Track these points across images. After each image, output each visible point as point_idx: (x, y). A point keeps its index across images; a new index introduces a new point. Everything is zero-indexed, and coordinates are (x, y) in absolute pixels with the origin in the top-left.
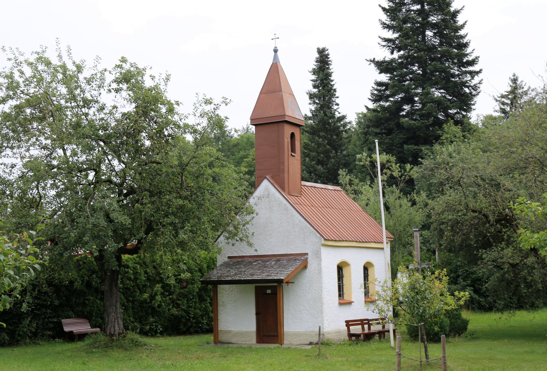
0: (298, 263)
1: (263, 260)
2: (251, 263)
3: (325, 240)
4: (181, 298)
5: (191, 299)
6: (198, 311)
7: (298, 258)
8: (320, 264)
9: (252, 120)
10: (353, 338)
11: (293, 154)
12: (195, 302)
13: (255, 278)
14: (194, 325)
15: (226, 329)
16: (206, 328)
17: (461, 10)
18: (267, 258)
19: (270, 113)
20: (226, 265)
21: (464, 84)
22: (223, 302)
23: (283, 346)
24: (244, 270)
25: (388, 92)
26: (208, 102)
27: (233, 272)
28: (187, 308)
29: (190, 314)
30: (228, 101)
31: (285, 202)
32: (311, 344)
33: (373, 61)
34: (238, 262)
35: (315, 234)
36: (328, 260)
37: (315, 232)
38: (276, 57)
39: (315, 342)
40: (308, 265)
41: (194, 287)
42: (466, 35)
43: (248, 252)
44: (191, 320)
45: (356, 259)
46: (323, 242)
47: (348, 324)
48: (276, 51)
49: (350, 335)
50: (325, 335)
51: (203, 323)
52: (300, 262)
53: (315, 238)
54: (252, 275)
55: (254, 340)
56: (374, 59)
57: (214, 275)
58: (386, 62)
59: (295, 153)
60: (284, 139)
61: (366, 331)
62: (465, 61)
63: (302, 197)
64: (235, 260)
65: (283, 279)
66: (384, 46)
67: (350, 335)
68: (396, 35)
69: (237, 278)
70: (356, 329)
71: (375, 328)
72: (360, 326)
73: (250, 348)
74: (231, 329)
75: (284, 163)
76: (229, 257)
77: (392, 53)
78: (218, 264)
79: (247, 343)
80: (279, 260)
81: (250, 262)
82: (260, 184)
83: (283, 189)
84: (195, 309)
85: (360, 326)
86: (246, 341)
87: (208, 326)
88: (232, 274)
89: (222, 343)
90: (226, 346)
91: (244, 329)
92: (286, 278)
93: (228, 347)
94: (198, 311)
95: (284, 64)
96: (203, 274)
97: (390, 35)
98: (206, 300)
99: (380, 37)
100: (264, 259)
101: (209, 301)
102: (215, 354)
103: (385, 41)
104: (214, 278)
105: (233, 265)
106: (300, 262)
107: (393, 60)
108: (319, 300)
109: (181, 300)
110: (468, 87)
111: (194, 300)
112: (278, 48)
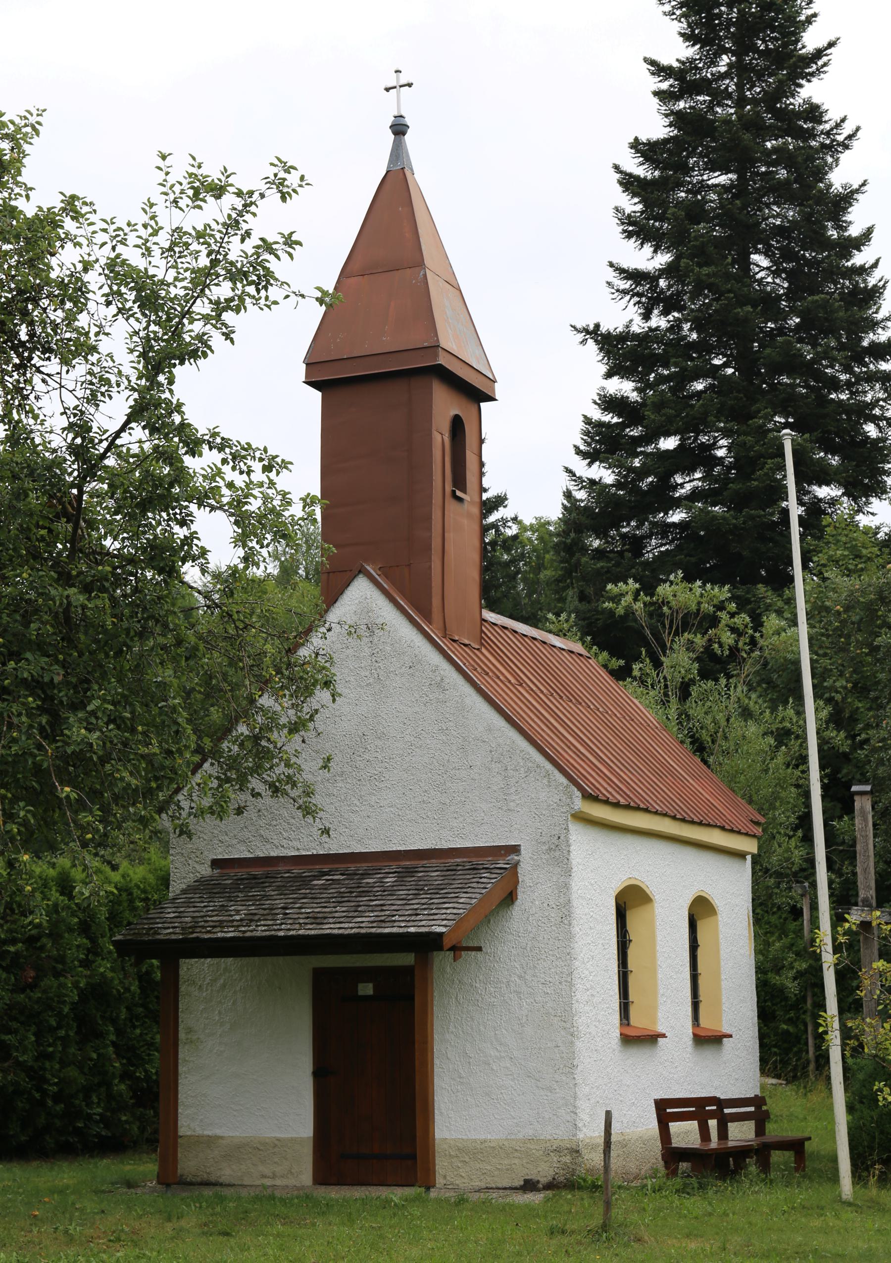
0: (489, 880)
1: (355, 870)
2: (304, 882)
3: (587, 796)
4: (14, 1025)
5: (53, 1030)
6: (72, 1072)
7: (486, 861)
8: (567, 886)
9: (311, 364)
10: (684, 1166)
11: (458, 493)
12: (65, 1040)
13: (328, 929)
14: (58, 1123)
15: (199, 1132)
16: (98, 1135)
17: (857, 191)
18: (364, 866)
19: (383, 339)
20: (202, 887)
21: (864, 412)
22: (190, 1031)
23: (433, 1194)
24: (280, 903)
25: (635, 432)
26: (206, 189)
27: (239, 911)
28: (37, 1059)
29: (46, 1081)
30: (292, 179)
31: (435, 658)
32: (529, 1186)
33: (594, 333)
34: (255, 877)
35: (548, 775)
36: (598, 866)
37: (548, 766)
38: (398, 152)
39: (544, 1180)
40: (520, 890)
41: (62, 986)
42: (875, 265)
43: (297, 839)
44: (50, 1103)
45: (675, 876)
46: (579, 804)
47: (667, 1111)
48: (399, 129)
49: (673, 1156)
50: (584, 1152)
51: (89, 1117)
52: (491, 875)
53: (548, 791)
54: (317, 920)
55: (305, 1176)
56: (597, 326)
57: (169, 926)
58: (636, 337)
59: (464, 491)
60: (430, 435)
61: (714, 1143)
62: (865, 343)
63: (484, 650)
64: (242, 872)
65: (441, 934)
66: (624, 292)
67: (673, 1156)
68: (663, 259)
69: (260, 931)
70: (685, 1133)
71: (741, 1133)
72: (695, 1123)
73: (269, 1204)
74: (218, 1132)
75: (429, 518)
76: (216, 863)
77: (646, 317)
78: (176, 887)
79: (278, 1182)
80: (410, 872)
81: (299, 877)
82: (342, 593)
83: (428, 618)
84: (63, 1064)
85: (695, 1123)
86: (274, 1176)
87: (107, 1127)
88: (237, 919)
89: (186, 1184)
90: (207, 1192)
91: (268, 1130)
92: (454, 929)
93: (221, 1199)
94: (72, 1072)
95: (425, 177)
96: (93, 940)
97: (647, 259)
98: (100, 1035)
99: (611, 265)
100: (352, 867)
101: (113, 1037)
102: (183, 1223)
103: (626, 278)
104: (167, 933)
105: (235, 887)
106: (491, 875)
107: (651, 335)
108: (563, 1018)
109: (15, 1032)
110: (875, 419)
111: (62, 1033)
112: (408, 121)
